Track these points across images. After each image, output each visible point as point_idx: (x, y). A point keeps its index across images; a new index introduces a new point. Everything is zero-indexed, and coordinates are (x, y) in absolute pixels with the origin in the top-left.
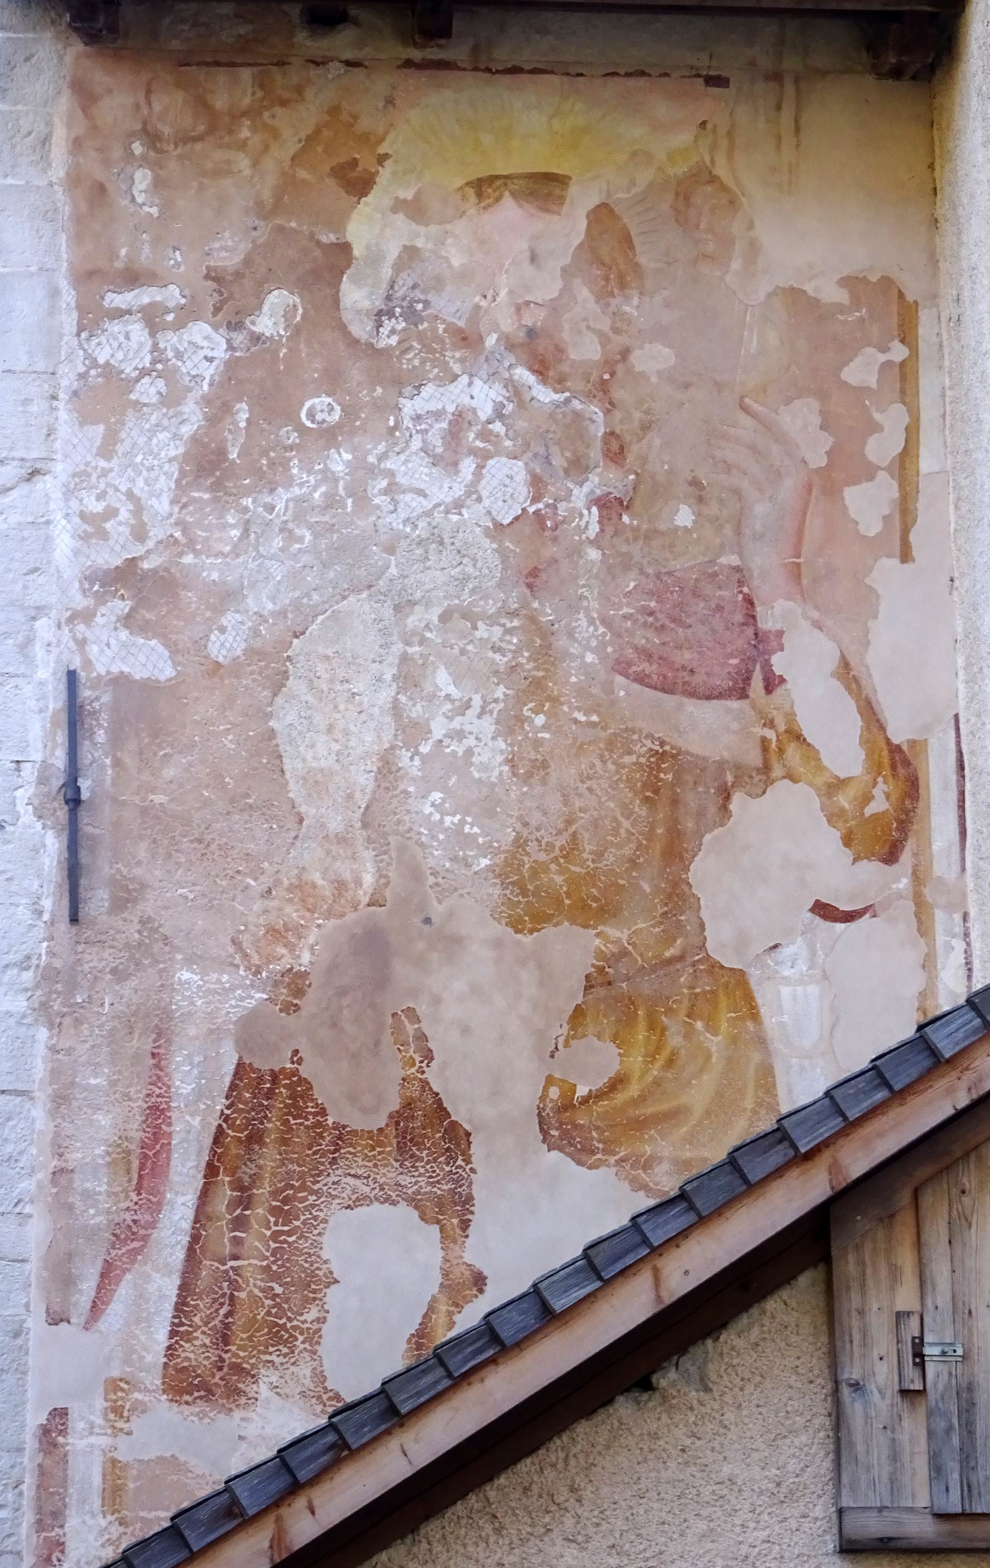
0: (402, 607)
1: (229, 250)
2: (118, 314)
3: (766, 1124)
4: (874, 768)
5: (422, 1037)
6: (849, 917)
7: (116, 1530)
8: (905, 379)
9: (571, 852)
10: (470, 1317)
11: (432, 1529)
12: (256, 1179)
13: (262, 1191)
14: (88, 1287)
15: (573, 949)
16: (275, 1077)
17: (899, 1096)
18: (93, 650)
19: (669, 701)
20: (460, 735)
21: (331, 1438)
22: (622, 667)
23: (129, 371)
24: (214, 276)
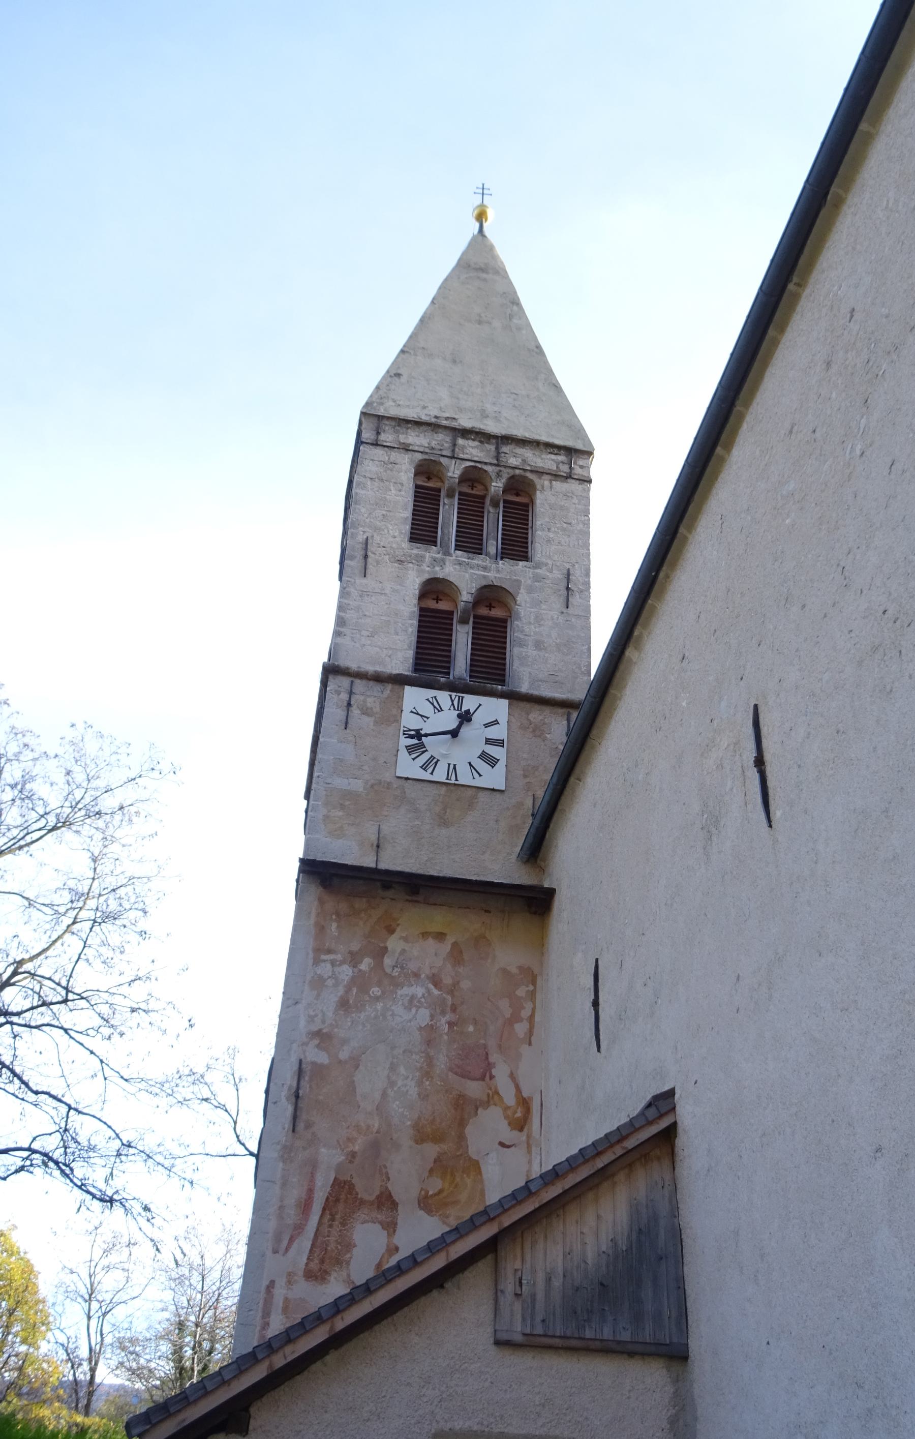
0: (393, 1048)
1: (355, 946)
2: (324, 961)
3: (481, 1208)
4: (518, 1104)
5: (387, 1173)
6: (509, 1147)
7: (284, 1320)
8: (532, 995)
9: (434, 1120)
10: (393, 1261)
11: (376, 1328)
12: (336, 1213)
13: (338, 1217)
14: (285, 1243)
15: (432, 1150)
16: (345, 1182)
17: (519, 1203)
18: (307, 1054)
19: (463, 1080)
20: (406, 1085)
21: (350, 1297)
22: (451, 1069)
23: (326, 976)
24: (351, 953)
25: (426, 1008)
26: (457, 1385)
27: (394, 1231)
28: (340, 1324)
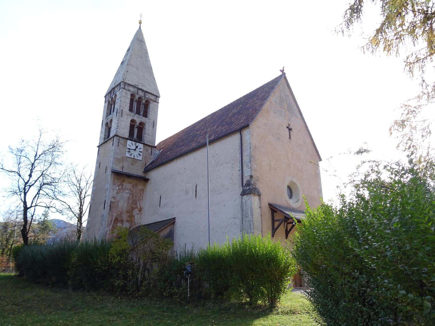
8: (143, 193)
15: (128, 214)
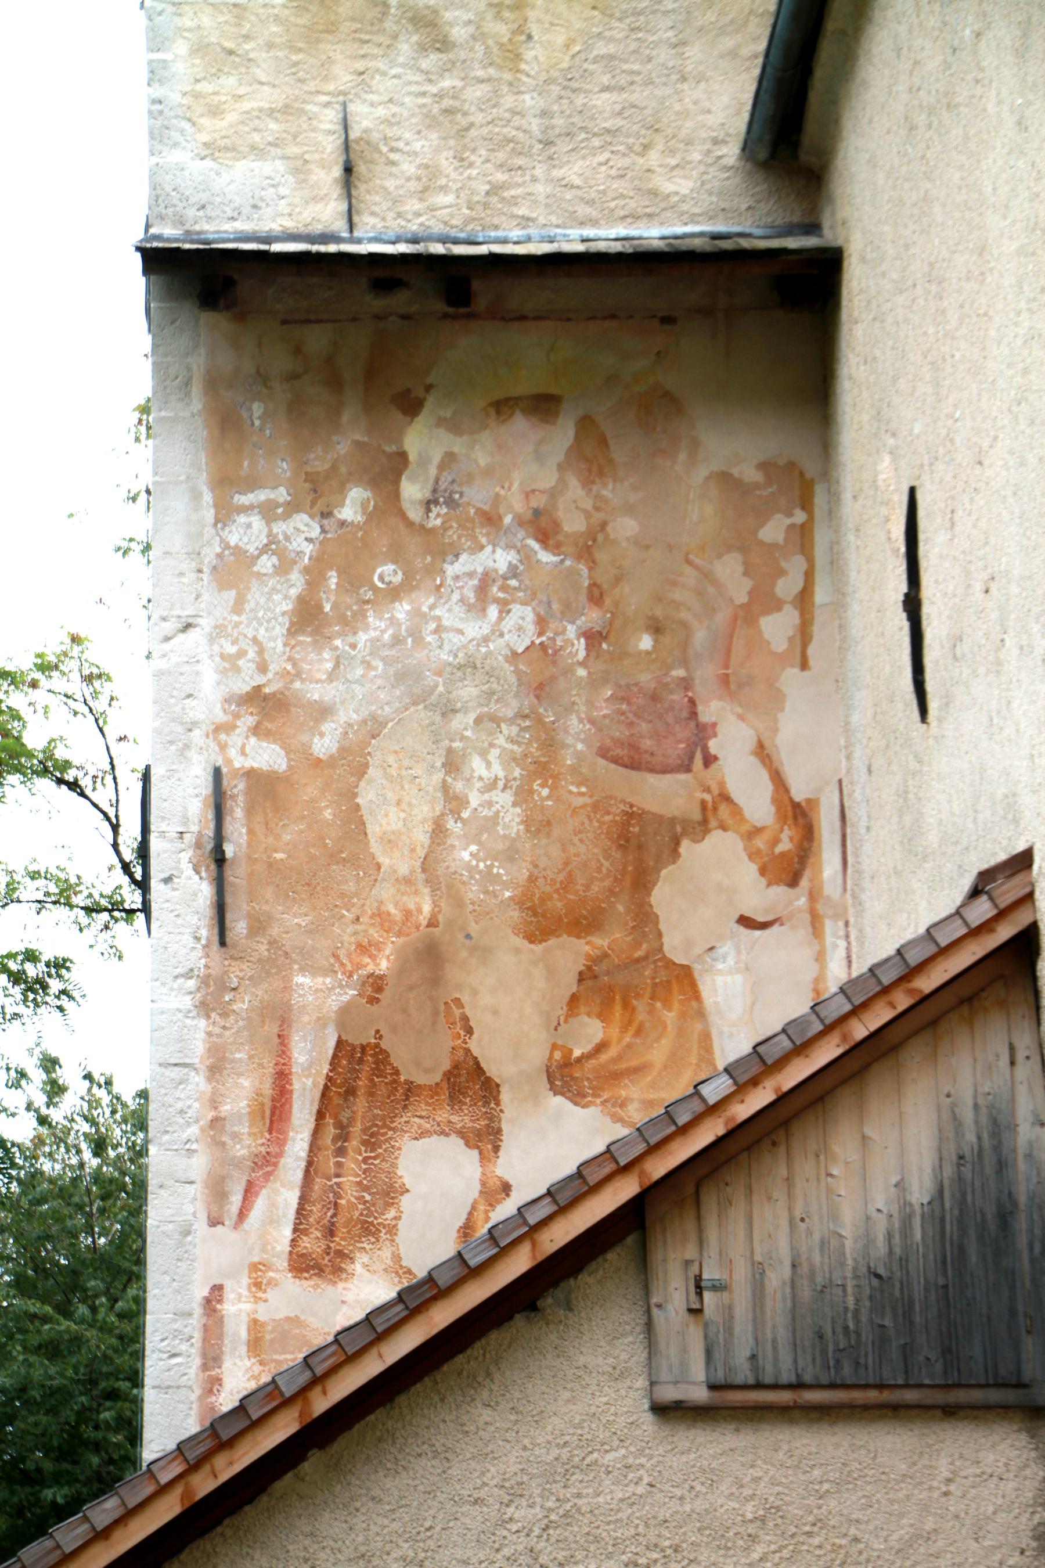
5: (465, 1019)
6: (764, 926)
7: (257, 1369)
8: (803, 538)
10: (506, 1209)
11: (402, 1400)
12: (351, 1120)
13: (356, 1129)
15: (570, 954)
16: (363, 1048)
19: (634, 774)
20: (490, 804)
23: (252, 549)
25: (524, 603)
26: (579, 1495)
27: (496, 1149)
28: (321, 1403)
